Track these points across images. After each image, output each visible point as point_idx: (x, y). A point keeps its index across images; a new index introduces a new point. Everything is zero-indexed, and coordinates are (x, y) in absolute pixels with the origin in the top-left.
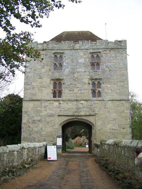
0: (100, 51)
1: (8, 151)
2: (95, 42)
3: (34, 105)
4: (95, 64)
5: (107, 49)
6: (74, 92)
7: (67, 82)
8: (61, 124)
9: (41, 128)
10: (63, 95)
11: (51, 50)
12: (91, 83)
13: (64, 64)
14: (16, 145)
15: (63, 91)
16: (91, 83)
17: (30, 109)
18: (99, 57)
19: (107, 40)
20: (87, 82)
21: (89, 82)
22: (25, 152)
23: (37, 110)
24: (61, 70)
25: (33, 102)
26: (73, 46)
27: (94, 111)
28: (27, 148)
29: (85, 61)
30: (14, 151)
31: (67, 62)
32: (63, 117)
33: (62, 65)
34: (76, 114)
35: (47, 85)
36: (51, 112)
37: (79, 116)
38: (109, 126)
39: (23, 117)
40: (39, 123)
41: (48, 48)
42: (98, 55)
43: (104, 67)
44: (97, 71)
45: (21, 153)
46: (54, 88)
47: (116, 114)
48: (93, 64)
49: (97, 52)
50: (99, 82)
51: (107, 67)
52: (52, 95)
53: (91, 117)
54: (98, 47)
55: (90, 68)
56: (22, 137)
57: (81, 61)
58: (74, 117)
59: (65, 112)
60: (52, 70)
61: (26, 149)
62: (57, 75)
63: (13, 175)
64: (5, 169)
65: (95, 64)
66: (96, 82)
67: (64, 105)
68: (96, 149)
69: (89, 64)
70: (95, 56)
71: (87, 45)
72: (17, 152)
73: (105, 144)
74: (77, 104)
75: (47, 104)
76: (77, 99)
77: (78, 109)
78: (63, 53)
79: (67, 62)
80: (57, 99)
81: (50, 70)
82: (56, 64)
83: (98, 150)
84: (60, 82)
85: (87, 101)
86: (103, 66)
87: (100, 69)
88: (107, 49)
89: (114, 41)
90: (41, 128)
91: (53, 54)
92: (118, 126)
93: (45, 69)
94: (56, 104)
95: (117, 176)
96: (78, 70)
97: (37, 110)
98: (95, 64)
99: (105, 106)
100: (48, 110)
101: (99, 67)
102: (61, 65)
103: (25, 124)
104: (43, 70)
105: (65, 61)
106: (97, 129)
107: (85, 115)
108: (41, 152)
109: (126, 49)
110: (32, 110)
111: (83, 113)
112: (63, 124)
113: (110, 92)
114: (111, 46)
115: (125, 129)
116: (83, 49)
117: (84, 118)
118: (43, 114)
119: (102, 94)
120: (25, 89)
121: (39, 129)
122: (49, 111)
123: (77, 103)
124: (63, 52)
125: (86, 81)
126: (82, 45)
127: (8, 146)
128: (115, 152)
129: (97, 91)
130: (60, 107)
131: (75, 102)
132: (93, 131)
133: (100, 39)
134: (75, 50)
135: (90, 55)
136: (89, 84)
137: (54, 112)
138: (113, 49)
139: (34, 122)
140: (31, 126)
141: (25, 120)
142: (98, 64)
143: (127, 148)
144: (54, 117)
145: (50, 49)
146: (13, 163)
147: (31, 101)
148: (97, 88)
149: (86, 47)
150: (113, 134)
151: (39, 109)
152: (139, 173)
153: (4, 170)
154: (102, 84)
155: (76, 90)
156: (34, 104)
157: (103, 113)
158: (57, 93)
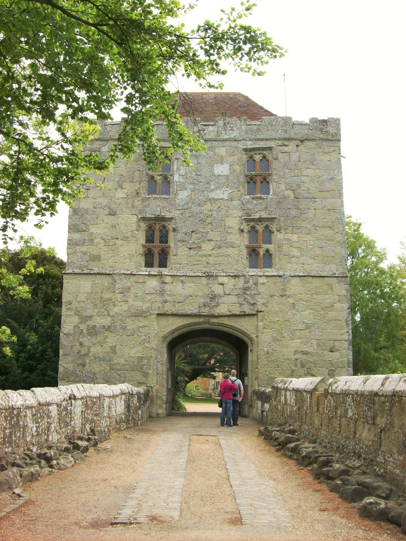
0: (269, 144)
1: (35, 404)
3: (94, 284)
5: (288, 139)
6: (201, 253)
8: (165, 338)
9: (111, 348)
10: (172, 259)
12: (246, 230)
13: (176, 178)
14: (195, 381)
15: (172, 250)
16: (246, 230)
17: (82, 297)
18: (268, 160)
19: (290, 118)
21: (242, 227)
22: (78, 407)
23: (101, 298)
24: (168, 193)
25: (92, 277)
27: (253, 304)
28: (82, 398)
29: (233, 171)
30: (49, 404)
31: (182, 172)
32: (171, 320)
33: (169, 182)
34: (206, 311)
35: (129, 234)
36: (139, 304)
37: (214, 316)
38: (295, 344)
39: (63, 318)
40: (107, 333)
42: (264, 157)
43: (283, 187)
44: (261, 198)
45: (67, 409)
46: (150, 239)
47: (311, 311)
48: (251, 180)
49: (263, 149)
50: (267, 227)
52: (142, 260)
53: (247, 319)
55: (243, 189)
56: (61, 369)
57: (222, 169)
58: (201, 320)
59: (177, 305)
60: (144, 194)
61: (78, 399)
62: (156, 207)
63: (51, 467)
64: (29, 449)
65: (258, 179)
66: (260, 228)
67: (177, 289)
68: (259, 403)
69: (242, 179)
70: (258, 158)
71: (238, 128)
72: (57, 406)
73: (286, 389)
75: (129, 284)
77: (213, 297)
80: (154, 271)
81: (137, 193)
82: (152, 178)
83: (267, 406)
84: (164, 227)
86: (278, 186)
87: (271, 192)
88: (288, 139)
90: (113, 349)
92: (318, 345)
93: (126, 191)
94: (153, 283)
95: (328, 468)
96: (211, 195)
97: (101, 298)
98: (257, 178)
99: (284, 290)
100: (131, 301)
101: (269, 188)
102: (166, 180)
103: (67, 335)
106: (261, 353)
107: (228, 313)
108: (116, 411)
109: (339, 141)
111: (223, 309)
113: (296, 252)
114: (303, 132)
115: (334, 353)
117: (226, 321)
119: (276, 260)
120: (71, 243)
121: (108, 349)
122: (135, 303)
125: (234, 222)
127: (33, 389)
128: (318, 409)
129: (262, 252)
130: (162, 292)
132: (251, 357)
133: (271, 114)
135: (245, 156)
136: (242, 231)
137: (145, 306)
138: (305, 140)
139: (93, 331)
140: (86, 340)
141: (68, 323)
142: (265, 179)
143: (353, 398)
146: (48, 436)
147: (85, 276)
148: (261, 243)
150: (303, 366)
151: (106, 295)
152: (387, 458)
153: (26, 452)
154: (275, 232)
155: (207, 247)
156: (95, 284)
158: (156, 253)
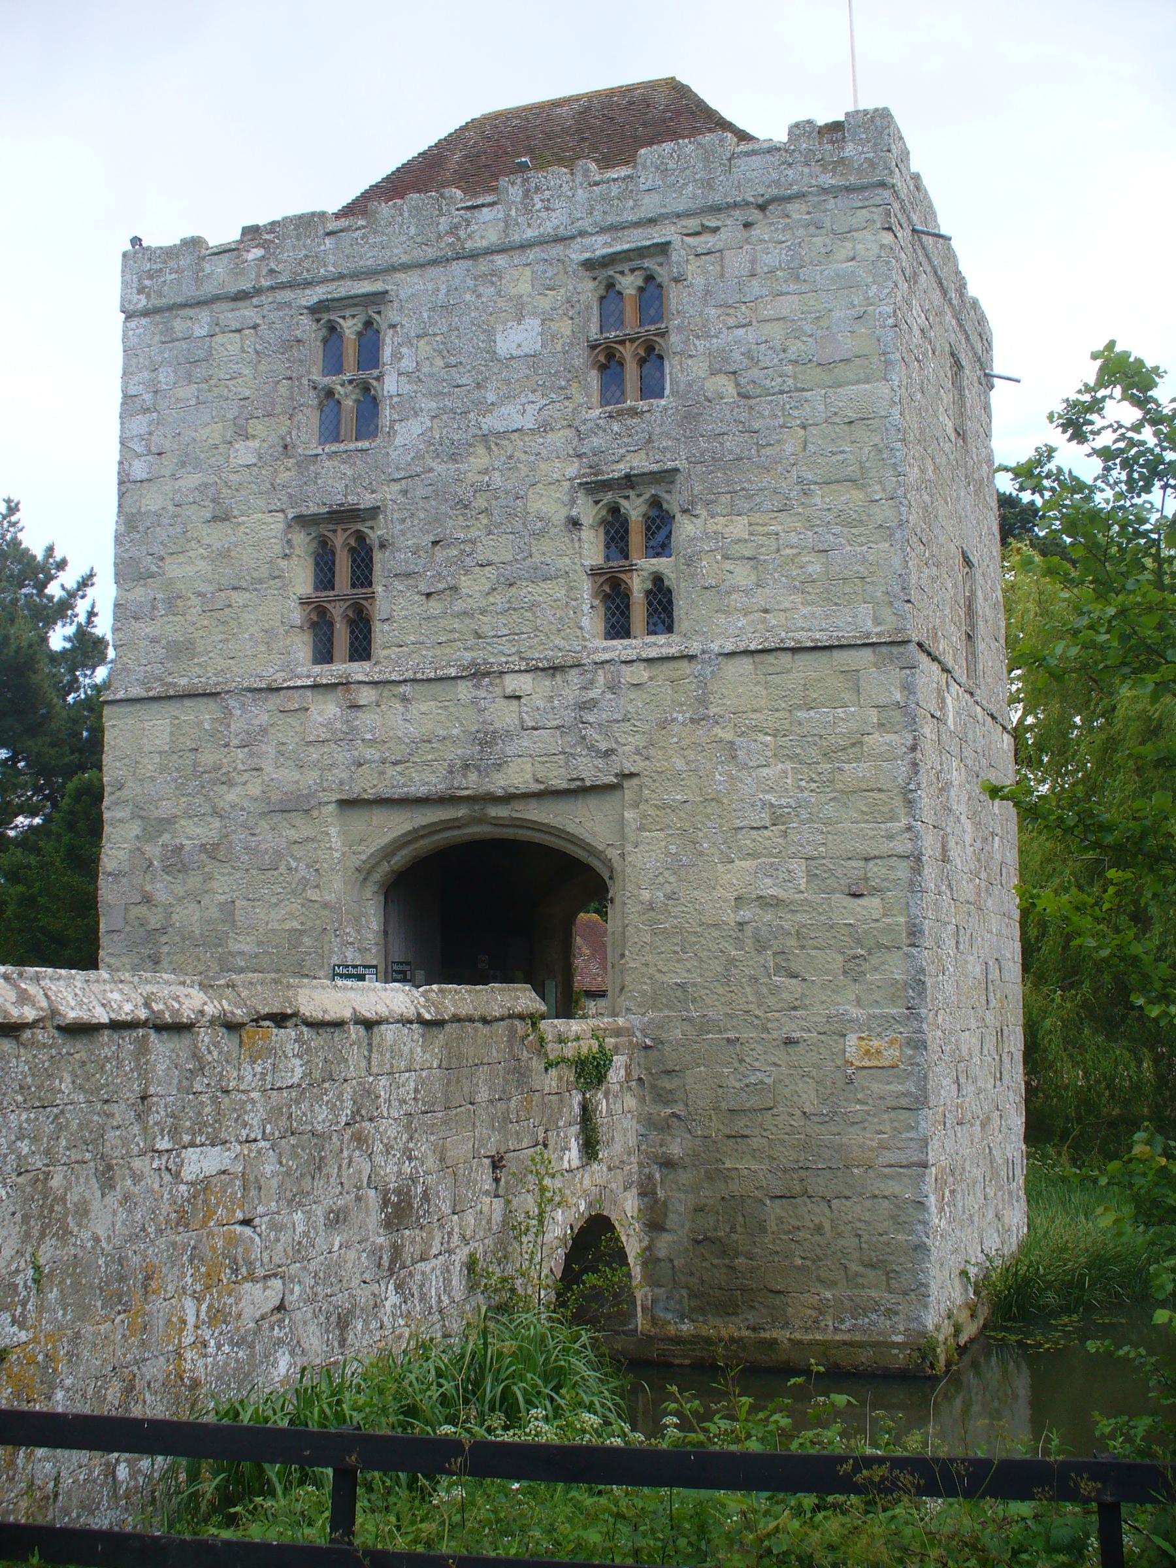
0: (657, 235)
2: (623, 171)
4: (628, 352)
5: (716, 209)
7: (401, 539)
8: (365, 872)
9: (222, 906)
11: (290, 285)
12: (587, 520)
17: (149, 766)
20: (559, 515)
23: (196, 764)
25: (172, 708)
26: (454, 229)
27: (609, 753)
29: (547, 337)
31: (407, 364)
32: (379, 816)
33: (374, 398)
34: (471, 783)
38: (738, 875)
39: (107, 829)
41: (272, 271)
43: (698, 368)
44: (634, 412)
47: (789, 765)
48: (607, 360)
51: (720, 365)
52: (301, 647)
53: (593, 801)
54: (650, 205)
57: (518, 338)
58: (461, 812)
59: (391, 771)
60: (307, 439)
62: (336, 481)
66: (635, 509)
69: (580, 357)
74: (474, 702)
75: (264, 718)
76: (479, 656)
77: (487, 739)
78: (378, 299)
79: (407, 364)
81: (285, 447)
82: (330, 393)
85: (554, 669)
86: (686, 368)
88: (716, 209)
89: (781, 136)
91: (306, 320)
92: (811, 876)
93: (256, 444)
96: (490, 422)
98: (628, 352)
99: (703, 701)
102: (370, 402)
103: (116, 875)
104: (244, 453)
105: (397, 356)
107: (536, 787)
110: (163, 769)
111: (518, 776)
112: (385, 867)
113: (742, 575)
115: (862, 902)
116: (523, 247)
117: (536, 813)
118: (232, 796)
121: (214, 913)
123: (482, 693)
124: (378, 286)
125: (550, 504)
126: (527, 209)
130: (349, 737)
131: (464, 690)
134: (473, 256)
135: (591, 285)
139: (176, 863)
140: (160, 890)
144: (315, 813)
145: (283, 278)
149: (555, 221)
151: (208, 758)
154: (678, 516)
156: (179, 727)
157: (680, 764)
158: (343, 625)
